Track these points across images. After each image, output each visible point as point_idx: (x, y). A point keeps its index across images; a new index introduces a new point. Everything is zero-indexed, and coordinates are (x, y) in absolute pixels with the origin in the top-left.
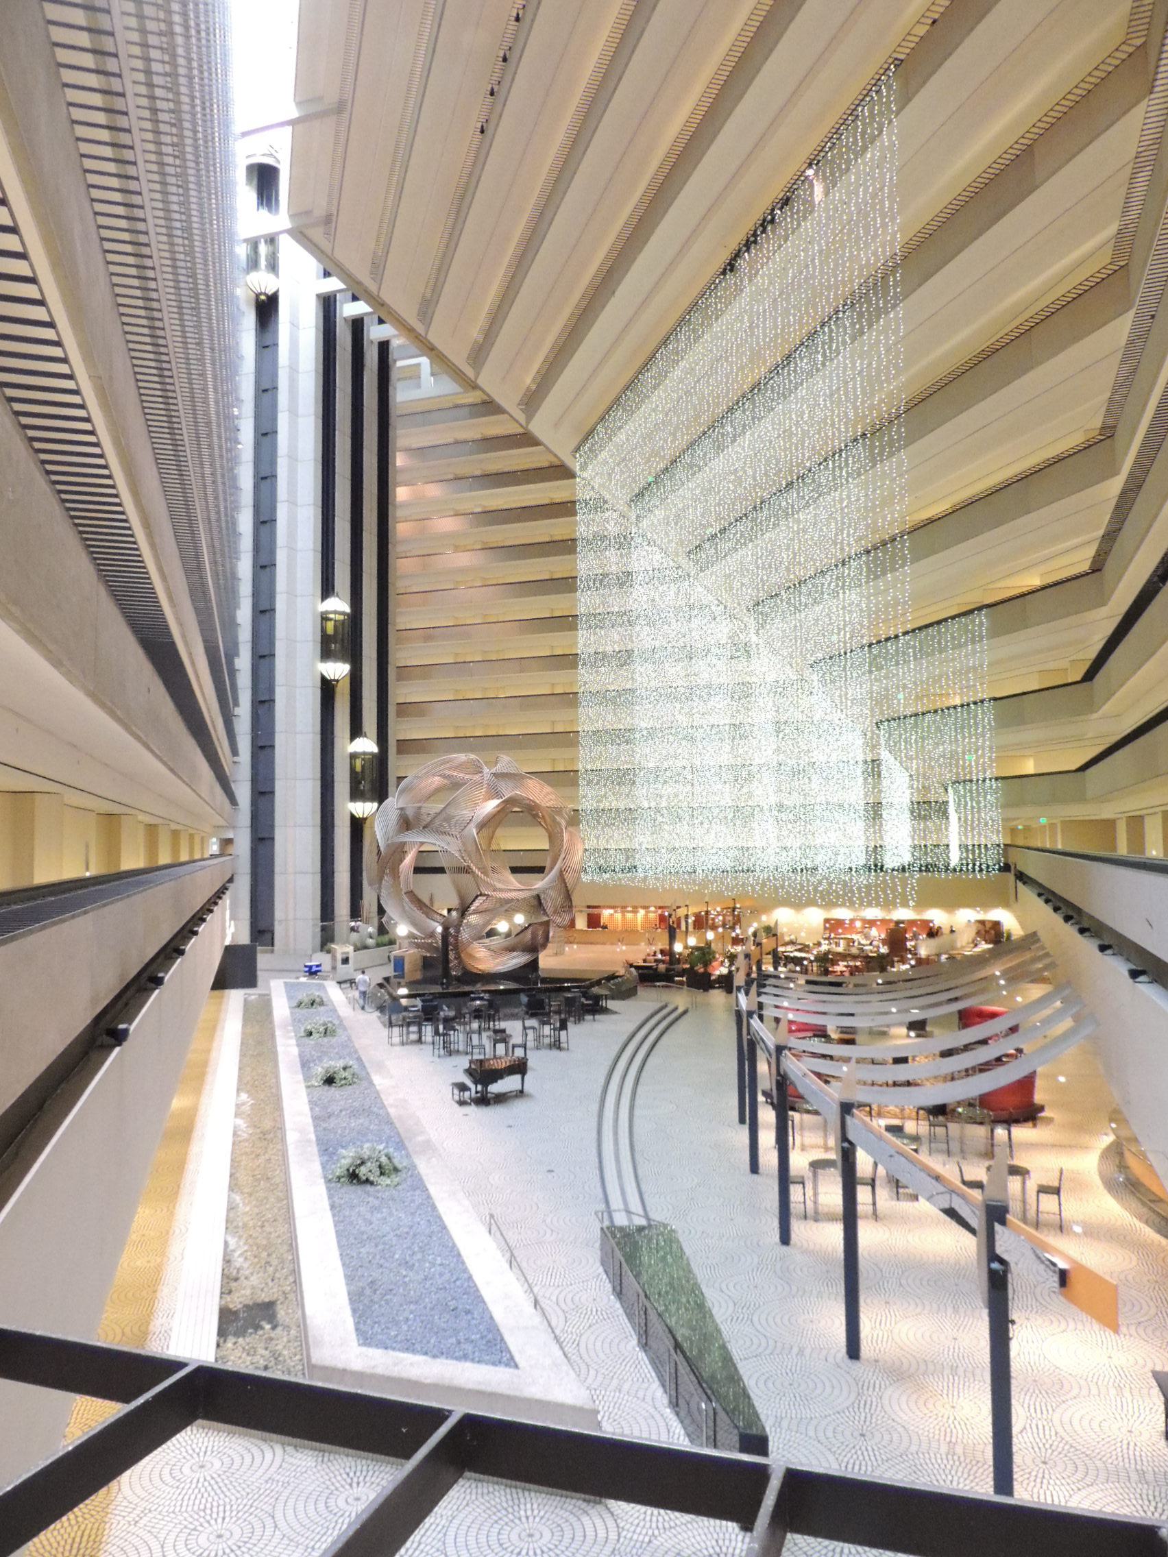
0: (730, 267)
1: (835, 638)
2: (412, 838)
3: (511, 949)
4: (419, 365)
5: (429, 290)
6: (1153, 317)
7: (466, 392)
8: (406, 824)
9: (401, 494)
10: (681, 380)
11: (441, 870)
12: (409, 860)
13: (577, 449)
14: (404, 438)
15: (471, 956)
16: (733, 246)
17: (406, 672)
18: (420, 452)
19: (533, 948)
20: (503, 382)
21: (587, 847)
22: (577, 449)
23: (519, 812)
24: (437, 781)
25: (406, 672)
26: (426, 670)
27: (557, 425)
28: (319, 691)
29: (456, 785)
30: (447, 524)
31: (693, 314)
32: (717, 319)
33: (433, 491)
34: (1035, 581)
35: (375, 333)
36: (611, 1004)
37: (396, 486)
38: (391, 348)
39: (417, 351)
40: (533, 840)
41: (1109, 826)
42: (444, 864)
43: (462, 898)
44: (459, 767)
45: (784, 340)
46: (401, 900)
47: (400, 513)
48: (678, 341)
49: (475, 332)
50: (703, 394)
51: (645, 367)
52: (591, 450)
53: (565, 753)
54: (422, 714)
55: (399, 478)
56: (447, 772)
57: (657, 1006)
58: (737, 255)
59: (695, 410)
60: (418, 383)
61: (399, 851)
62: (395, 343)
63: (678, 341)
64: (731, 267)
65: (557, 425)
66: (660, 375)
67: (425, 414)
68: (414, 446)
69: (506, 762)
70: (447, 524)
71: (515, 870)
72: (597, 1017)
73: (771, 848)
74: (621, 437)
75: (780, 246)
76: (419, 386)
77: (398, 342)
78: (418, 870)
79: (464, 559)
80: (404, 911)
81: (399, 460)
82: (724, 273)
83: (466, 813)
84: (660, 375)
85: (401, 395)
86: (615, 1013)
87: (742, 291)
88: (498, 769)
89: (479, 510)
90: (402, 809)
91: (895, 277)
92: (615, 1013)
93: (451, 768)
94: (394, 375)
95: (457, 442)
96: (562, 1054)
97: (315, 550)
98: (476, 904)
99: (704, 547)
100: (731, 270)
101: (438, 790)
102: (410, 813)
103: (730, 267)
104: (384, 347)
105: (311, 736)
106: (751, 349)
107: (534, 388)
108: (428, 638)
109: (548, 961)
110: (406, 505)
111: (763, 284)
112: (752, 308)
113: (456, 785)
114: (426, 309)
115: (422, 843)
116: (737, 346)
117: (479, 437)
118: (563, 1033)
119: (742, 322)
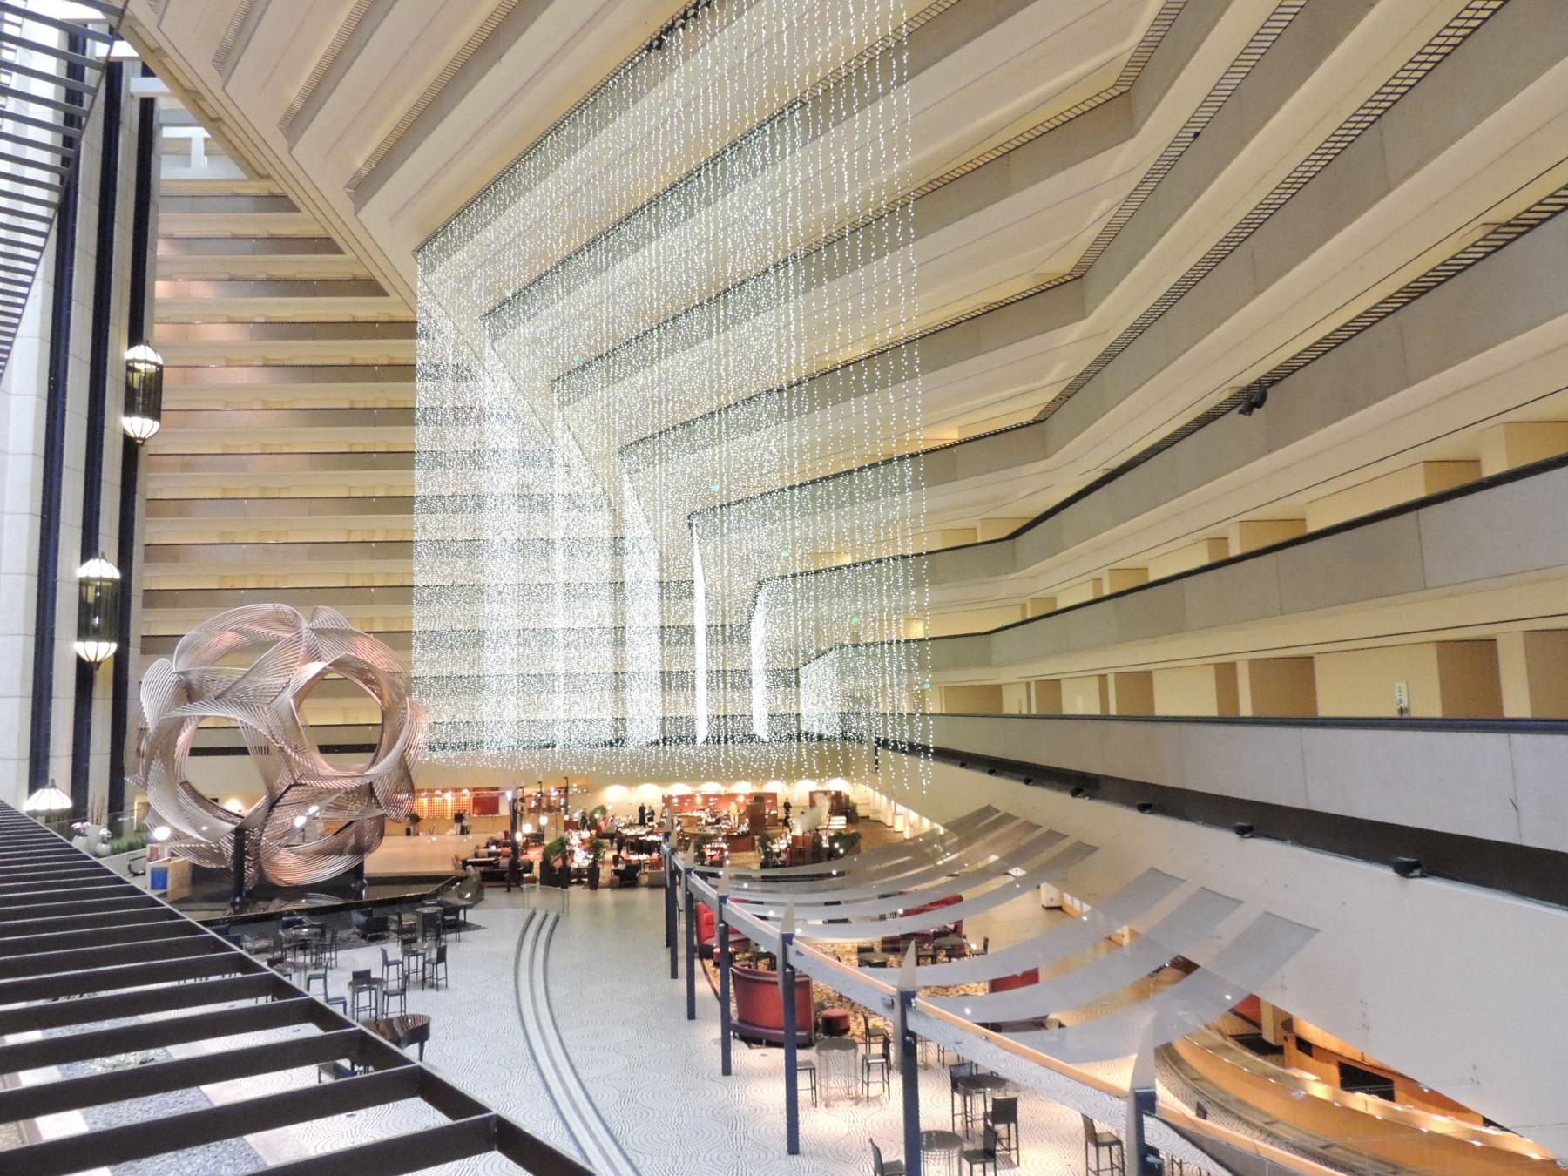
0: (657, 44)
1: (716, 488)
2: (195, 711)
3: (325, 853)
4: (188, 140)
5: (231, 33)
6: (1197, 135)
7: (251, 178)
8: (189, 692)
9: (160, 289)
10: (579, 171)
11: (242, 751)
12: (183, 739)
13: (420, 249)
14: (167, 223)
15: (274, 865)
16: (662, 20)
17: (158, 507)
18: (187, 243)
19: (360, 850)
20: (320, 165)
21: (429, 718)
22: (420, 249)
23: (347, 677)
24: (229, 638)
25: (158, 507)
26: (180, 507)
27: (394, 217)
28: (39, 520)
29: (260, 645)
30: (220, 333)
31: (600, 96)
32: (634, 102)
33: (202, 291)
34: (953, 435)
35: (137, 85)
36: (471, 916)
37: (155, 279)
38: (156, 109)
39: (192, 119)
40: (365, 712)
41: (996, 690)
42: (246, 742)
43: (270, 789)
44: (261, 621)
45: (733, 125)
46: (175, 795)
47: (159, 312)
48: (576, 126)
49: (293, 95)
50: (614, 187)
51: (527, 154)
52: (440, 249)
53: (395, 611)
54: (176, 559)
55: (160, 270)
56: (245, 626)
57: (528, 912)
58: (669, 29)
59: (600, 205)
60: (189, 155)
61: (171, 729)
62: (162, 105)
63: (576, 126)
64: (656, 45)
65: (394, 217)
66: (548, 164)
67: (197, 198)
68: (178, 234)
69: (328, 616)
70: (220, 333)
71: (325, 749)
72: (462, 934)
73: (573, 717)
74: (488, 234)
75: (730, 22)
76: (188, 165)
77: (168, 104)
78: (195, 752)
79: (240, 376)
80: (181, 809)
81: (161, 250)
82: (650, 48)
83: (272, 681)
84: (548, 164)
85: (167, 171)
86: (478, 928)
87: (672, 71)
88: (316, 624)
89: (261, 319)
90: (182, 673)
91: (900, 61)
92: (478, 928)
93: (252, 621)
94: (158, 146)
95: (234, 237)
96: (442, 993)
97: (41, 338)
98: (288, 797)
99: (566, 379)
100: (659, 47)
101: (231, 651)
102: (193, 678)
103: (657, 44)
104: (147, 105)
105: (24, 577)
106: (687, 136)
107: (366, 172)
108: (186, 467)
109: (374, 864)
110: (168, 304)
111: (705, 63)
112: (688, 90)
113: (260, 645)
114: (226, 59)
115: (203, 718)
116: (665, 133)
117: (264, 234)
118: (441, 966)
119: (673, 106)
